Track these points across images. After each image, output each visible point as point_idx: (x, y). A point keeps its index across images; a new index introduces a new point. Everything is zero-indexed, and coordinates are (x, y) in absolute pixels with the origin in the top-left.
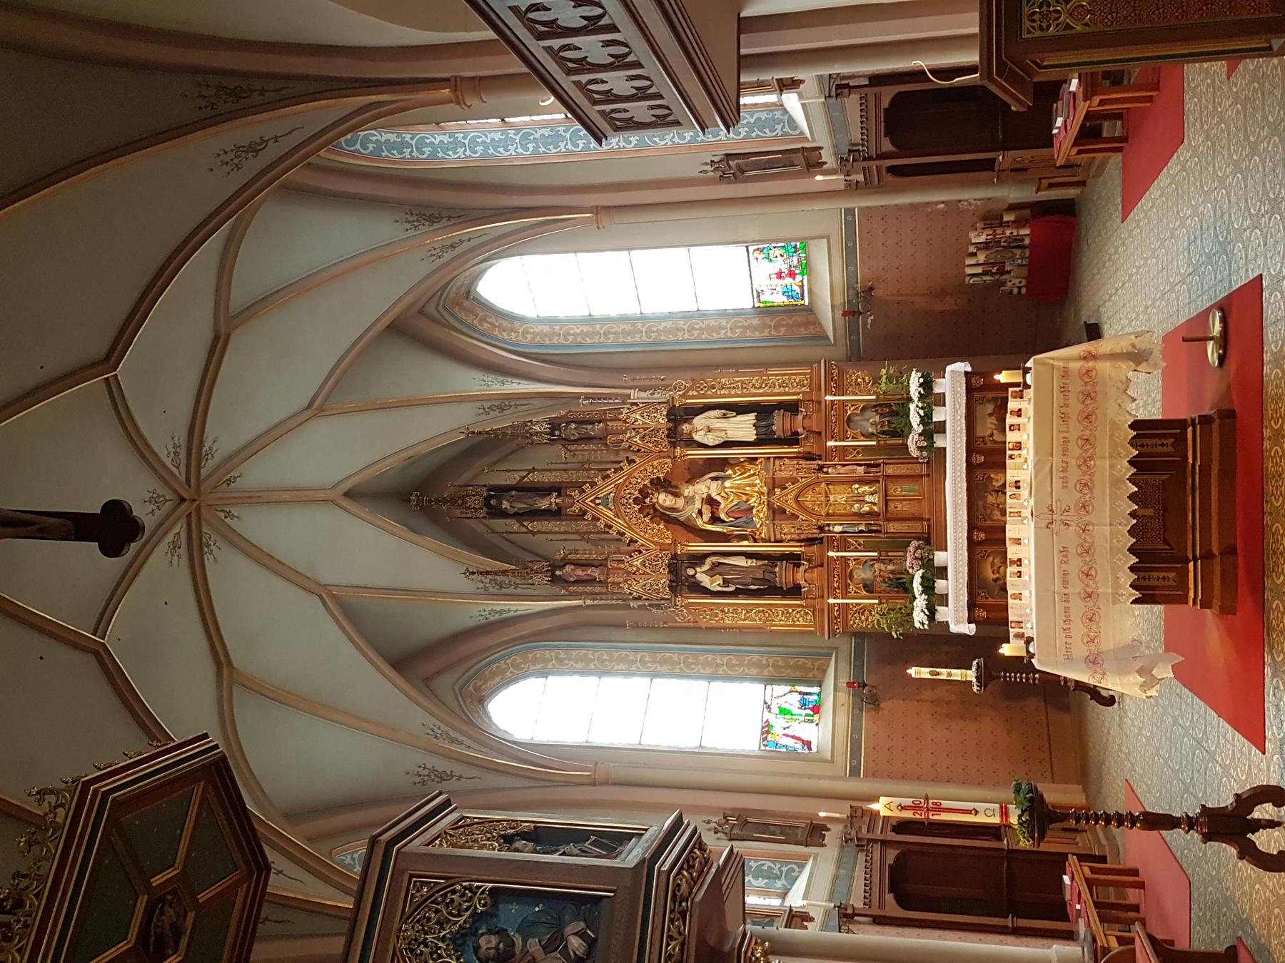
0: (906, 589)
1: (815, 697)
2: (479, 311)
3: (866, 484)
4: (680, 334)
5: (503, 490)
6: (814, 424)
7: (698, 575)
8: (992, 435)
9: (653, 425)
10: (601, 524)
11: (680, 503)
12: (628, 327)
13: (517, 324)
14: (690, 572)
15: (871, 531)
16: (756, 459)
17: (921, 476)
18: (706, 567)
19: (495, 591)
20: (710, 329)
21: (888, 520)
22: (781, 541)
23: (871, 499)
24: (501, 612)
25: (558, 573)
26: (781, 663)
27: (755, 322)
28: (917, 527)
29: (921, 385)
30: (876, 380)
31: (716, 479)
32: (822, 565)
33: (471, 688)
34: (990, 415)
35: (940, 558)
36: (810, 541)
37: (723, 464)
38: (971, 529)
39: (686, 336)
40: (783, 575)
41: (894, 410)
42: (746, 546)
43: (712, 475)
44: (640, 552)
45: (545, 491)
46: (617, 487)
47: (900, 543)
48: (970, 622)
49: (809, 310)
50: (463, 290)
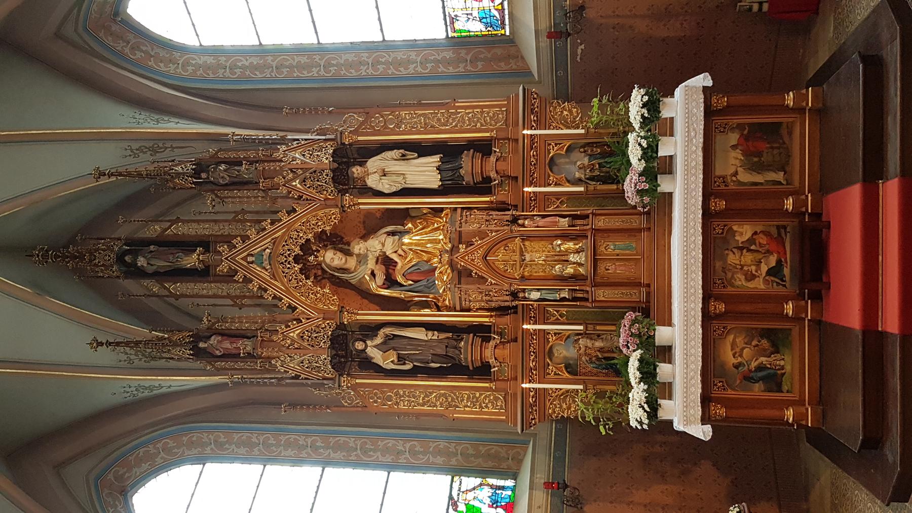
0: (618, 371)
1: (509, 493)
2: (130, 37)
3: (572, 239)
4: (363, 68)
5: (137, 245)
6: (510, 166)
7: (369, 350)
8: (736, 174)
9: (312, 163)
10: (254, 287)
11: (352, 263)
12: (304, 60)
13: (177, 55)
14: (359, 346)
15: (575, 299)
16: (442, 210)
17: (639, 230)
18: (379, 340)
19: (142, 364)
20: (398, 64)
21: (596, 285)
22: (469, 310)
23: (577, 258)
24: (151, 388)
25: (202, 345)
26: (471, 451)
27: (449, 55)
28: (636, 295)
29: (644, 106)
30: (585, 116)
31: (393, 234)
32: (515, 340)
33: (111, 476)
34: (734, 147)
35: (662, 334)
36: (502, 311)
37: (399, 217)
38: (706, 299)
39: (370, 71)
40: (469, 351)
41: (607, 152)
42: (427, 315)
43: (390, 228)
44: (299, 321)
45: (187, 245)
46: (274, 242)
47: (611, 315)
48: (704, 421)
49: (511, 41)
50: (108, 9)
